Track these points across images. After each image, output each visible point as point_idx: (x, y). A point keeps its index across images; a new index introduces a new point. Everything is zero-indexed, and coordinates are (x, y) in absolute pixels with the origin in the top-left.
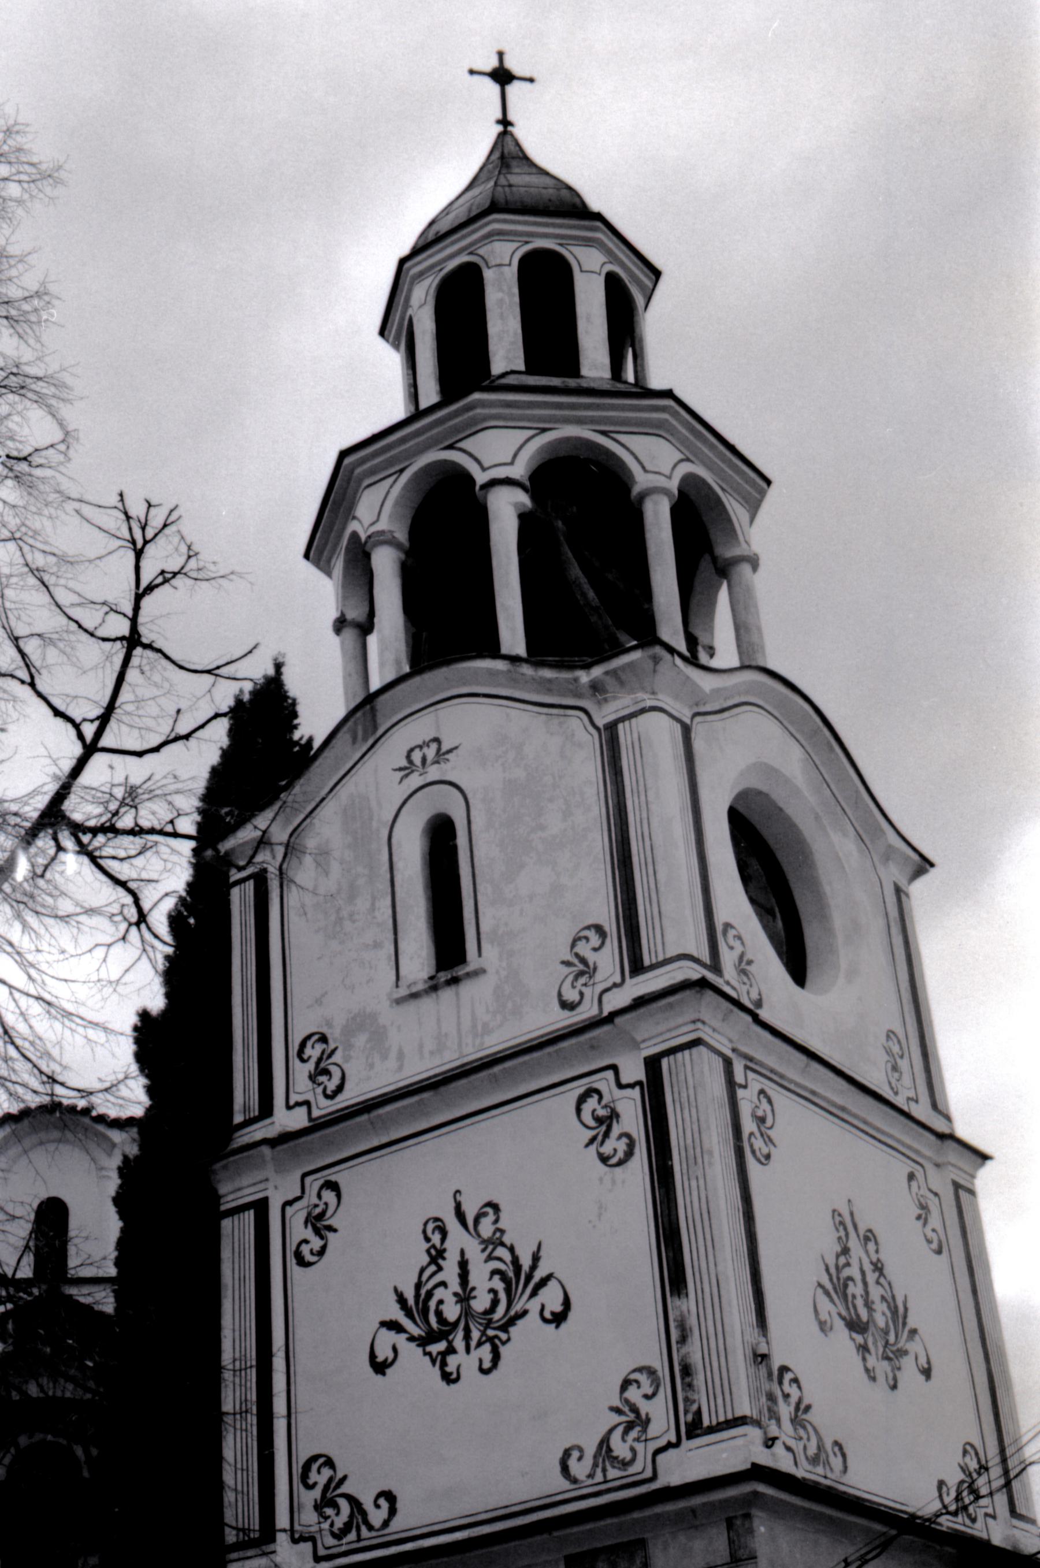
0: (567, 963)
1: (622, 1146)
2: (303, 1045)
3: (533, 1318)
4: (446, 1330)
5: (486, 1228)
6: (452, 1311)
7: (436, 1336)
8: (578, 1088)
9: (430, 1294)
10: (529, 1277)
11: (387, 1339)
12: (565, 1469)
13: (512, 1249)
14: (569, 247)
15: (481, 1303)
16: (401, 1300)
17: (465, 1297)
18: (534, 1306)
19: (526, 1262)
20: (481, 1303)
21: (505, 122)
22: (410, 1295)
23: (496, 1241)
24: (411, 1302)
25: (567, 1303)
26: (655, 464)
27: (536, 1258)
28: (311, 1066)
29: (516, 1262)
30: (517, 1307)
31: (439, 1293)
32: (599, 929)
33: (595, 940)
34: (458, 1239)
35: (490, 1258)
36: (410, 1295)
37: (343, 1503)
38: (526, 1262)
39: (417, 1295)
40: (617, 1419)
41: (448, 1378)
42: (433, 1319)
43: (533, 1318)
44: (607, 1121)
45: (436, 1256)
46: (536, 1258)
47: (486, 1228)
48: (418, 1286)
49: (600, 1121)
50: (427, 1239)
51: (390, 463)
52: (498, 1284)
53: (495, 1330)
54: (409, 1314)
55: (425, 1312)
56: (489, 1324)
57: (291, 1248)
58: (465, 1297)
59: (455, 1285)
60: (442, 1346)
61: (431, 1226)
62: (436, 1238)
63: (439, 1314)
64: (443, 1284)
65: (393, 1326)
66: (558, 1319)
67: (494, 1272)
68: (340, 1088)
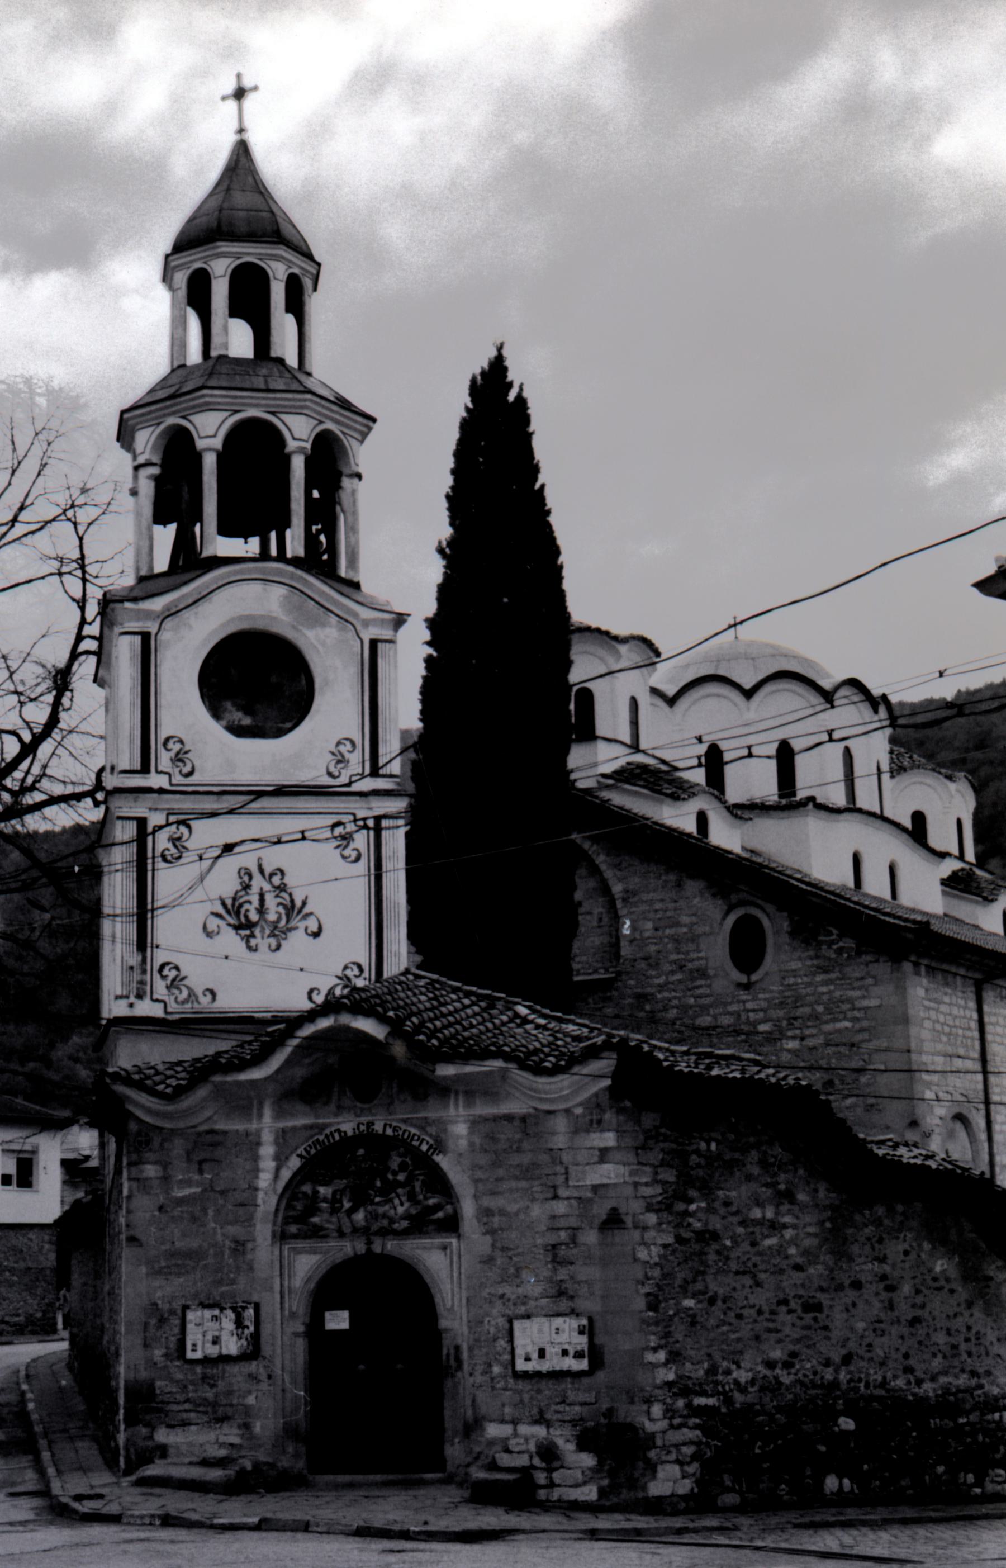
0: (333, 754)
1: (170, 745)
2: (167, 740)
3: (301, 932)
4: (250, 925)
5: (276, 880)
6: (254, 917)
7: (244, 926)
8: (334, 819)
9: (241, 906)
10: (300, 911)
11: (213, 923)
12: (310, 998)
13: (290, 895)
14: (283, 416)
15: (272, 917)
16: (224, 904)
17: (262, 910)
18: (302, 925)
19: (298, 903)
20: (272, 917)
21: (241, 131)
22: (229, 902)
23: (282, 888)
24: (230, 906)
25: (320, 928)
26: (298, 431)
27: (304, 903)
28: (172, 754)
29: (292, 901)
30: (292, 924)
31: (246, 906)
32: (353, 743)
33: (349, 746)
34: (258, 883)
35: (277, 896)
36: (229, 902)
37: (184, 989)
38: (298, 903)
39: (233, 905)
40: (338, 981)
41: (250, 948)
42: (243, 919)
43: (301, 932)
44: (179, 759)
45: (246, 887)
46: (304, 903)
47: (276, 880)
48: (234, 899)
49: (181, 760)
50: (241, 877)
51: (156, 418)
52: (281, 909)
53: (279, 933)
54: (228, 912)
55: (238, 913)
56: (276, 928)
57: (158, 853)
58: (262, 910)
59: (256, 903)
60: (248, 932)
61: (243, 872)
62: (246, 878)
63: (246, 917)
64: (250, 902)
65: (218, 915)
66: (316, 935)
67: (280, 904)
68: (190, 774)
